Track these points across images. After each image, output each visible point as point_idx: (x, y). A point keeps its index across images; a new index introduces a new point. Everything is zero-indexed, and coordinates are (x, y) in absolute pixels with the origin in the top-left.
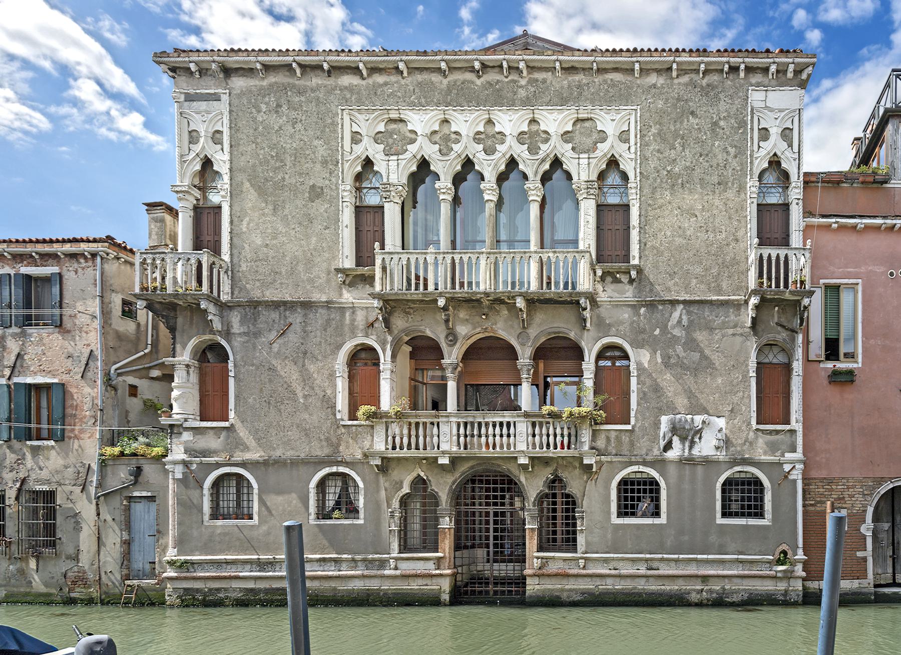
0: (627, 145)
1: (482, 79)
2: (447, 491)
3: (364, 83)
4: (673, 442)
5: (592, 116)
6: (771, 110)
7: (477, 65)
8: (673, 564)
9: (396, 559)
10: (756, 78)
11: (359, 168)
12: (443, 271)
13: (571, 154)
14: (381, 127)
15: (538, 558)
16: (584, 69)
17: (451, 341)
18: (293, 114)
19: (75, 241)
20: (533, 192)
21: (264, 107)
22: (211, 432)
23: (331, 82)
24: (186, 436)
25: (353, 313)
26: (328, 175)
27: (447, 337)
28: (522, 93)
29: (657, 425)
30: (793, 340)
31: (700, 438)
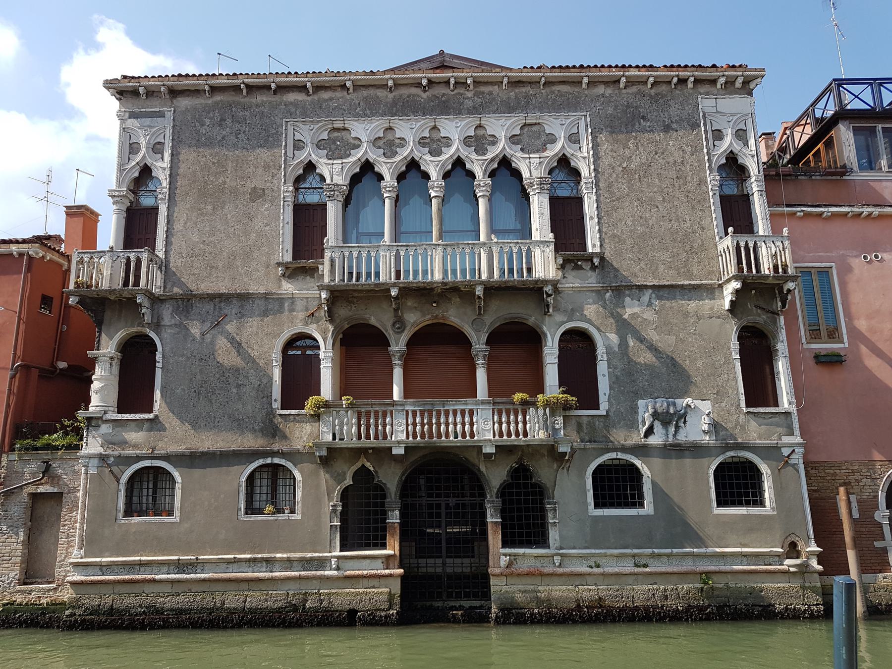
1: (427, 93)
2: (396, 482)
3: (309, 98)
4: (655, 427)
6: (724, 114)
7: (424, 82)
8: (665, 559)
9: (338, 558)
10: (703, 89)
14: (325, 136)
15: (505, 555)
16: (530, 83)
17: (398, 328)
18: (237, 126)
19: (10, 242)
21: (207, 122)
22: (133, 424)
23: (277, 98)
24: (105, 429)
25: (293, 303)
26: (270, 178)
27: (394, 325)
28: (469, 103)
29: (634, 409)
30: (775, 322)
31: (685, 423)
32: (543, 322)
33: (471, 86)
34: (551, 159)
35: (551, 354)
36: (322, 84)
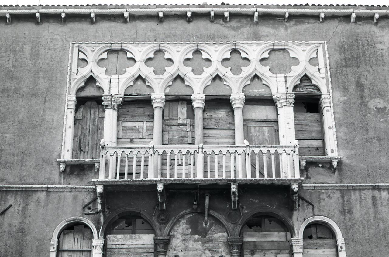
0: (317, 68)
5: (286, 47)
11: (83, 84)
12: (154, 162)
13: (269, 74)
17: (163, 220)
20: (237, 102)
32: (291, 217)
33: (228, 19)
34: (78, 81)
35: (297, 245)
36: (278, 14)
